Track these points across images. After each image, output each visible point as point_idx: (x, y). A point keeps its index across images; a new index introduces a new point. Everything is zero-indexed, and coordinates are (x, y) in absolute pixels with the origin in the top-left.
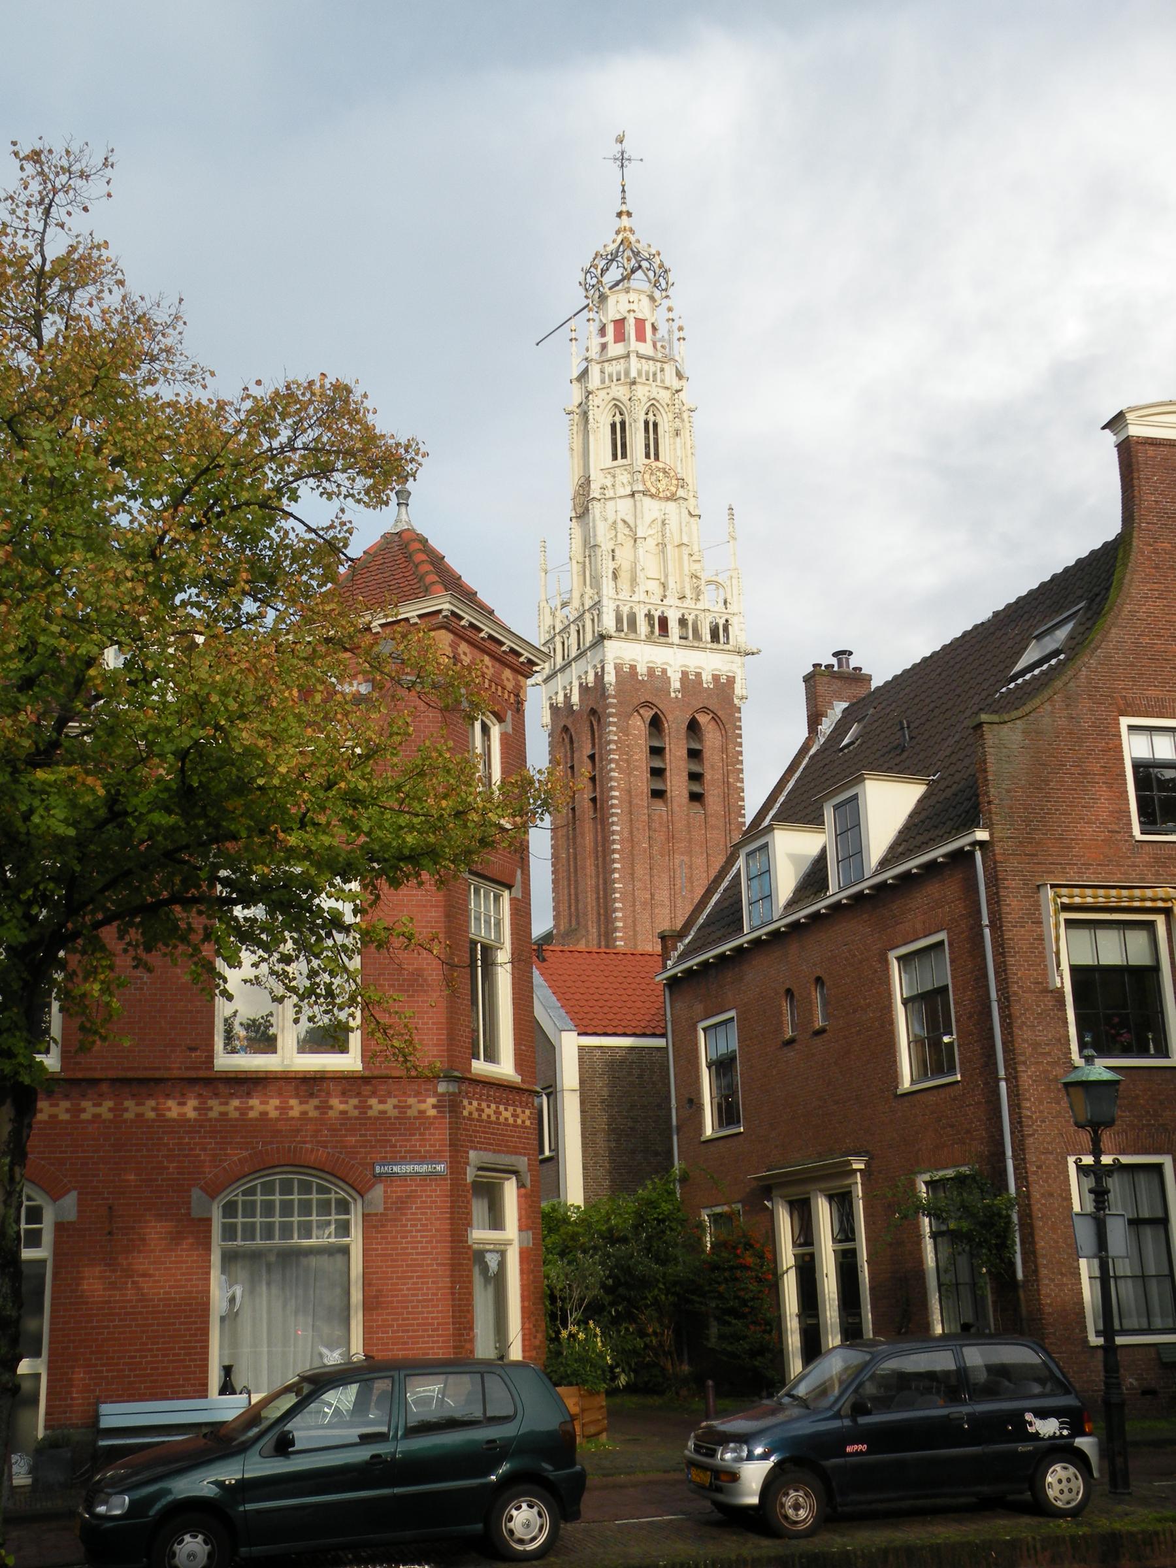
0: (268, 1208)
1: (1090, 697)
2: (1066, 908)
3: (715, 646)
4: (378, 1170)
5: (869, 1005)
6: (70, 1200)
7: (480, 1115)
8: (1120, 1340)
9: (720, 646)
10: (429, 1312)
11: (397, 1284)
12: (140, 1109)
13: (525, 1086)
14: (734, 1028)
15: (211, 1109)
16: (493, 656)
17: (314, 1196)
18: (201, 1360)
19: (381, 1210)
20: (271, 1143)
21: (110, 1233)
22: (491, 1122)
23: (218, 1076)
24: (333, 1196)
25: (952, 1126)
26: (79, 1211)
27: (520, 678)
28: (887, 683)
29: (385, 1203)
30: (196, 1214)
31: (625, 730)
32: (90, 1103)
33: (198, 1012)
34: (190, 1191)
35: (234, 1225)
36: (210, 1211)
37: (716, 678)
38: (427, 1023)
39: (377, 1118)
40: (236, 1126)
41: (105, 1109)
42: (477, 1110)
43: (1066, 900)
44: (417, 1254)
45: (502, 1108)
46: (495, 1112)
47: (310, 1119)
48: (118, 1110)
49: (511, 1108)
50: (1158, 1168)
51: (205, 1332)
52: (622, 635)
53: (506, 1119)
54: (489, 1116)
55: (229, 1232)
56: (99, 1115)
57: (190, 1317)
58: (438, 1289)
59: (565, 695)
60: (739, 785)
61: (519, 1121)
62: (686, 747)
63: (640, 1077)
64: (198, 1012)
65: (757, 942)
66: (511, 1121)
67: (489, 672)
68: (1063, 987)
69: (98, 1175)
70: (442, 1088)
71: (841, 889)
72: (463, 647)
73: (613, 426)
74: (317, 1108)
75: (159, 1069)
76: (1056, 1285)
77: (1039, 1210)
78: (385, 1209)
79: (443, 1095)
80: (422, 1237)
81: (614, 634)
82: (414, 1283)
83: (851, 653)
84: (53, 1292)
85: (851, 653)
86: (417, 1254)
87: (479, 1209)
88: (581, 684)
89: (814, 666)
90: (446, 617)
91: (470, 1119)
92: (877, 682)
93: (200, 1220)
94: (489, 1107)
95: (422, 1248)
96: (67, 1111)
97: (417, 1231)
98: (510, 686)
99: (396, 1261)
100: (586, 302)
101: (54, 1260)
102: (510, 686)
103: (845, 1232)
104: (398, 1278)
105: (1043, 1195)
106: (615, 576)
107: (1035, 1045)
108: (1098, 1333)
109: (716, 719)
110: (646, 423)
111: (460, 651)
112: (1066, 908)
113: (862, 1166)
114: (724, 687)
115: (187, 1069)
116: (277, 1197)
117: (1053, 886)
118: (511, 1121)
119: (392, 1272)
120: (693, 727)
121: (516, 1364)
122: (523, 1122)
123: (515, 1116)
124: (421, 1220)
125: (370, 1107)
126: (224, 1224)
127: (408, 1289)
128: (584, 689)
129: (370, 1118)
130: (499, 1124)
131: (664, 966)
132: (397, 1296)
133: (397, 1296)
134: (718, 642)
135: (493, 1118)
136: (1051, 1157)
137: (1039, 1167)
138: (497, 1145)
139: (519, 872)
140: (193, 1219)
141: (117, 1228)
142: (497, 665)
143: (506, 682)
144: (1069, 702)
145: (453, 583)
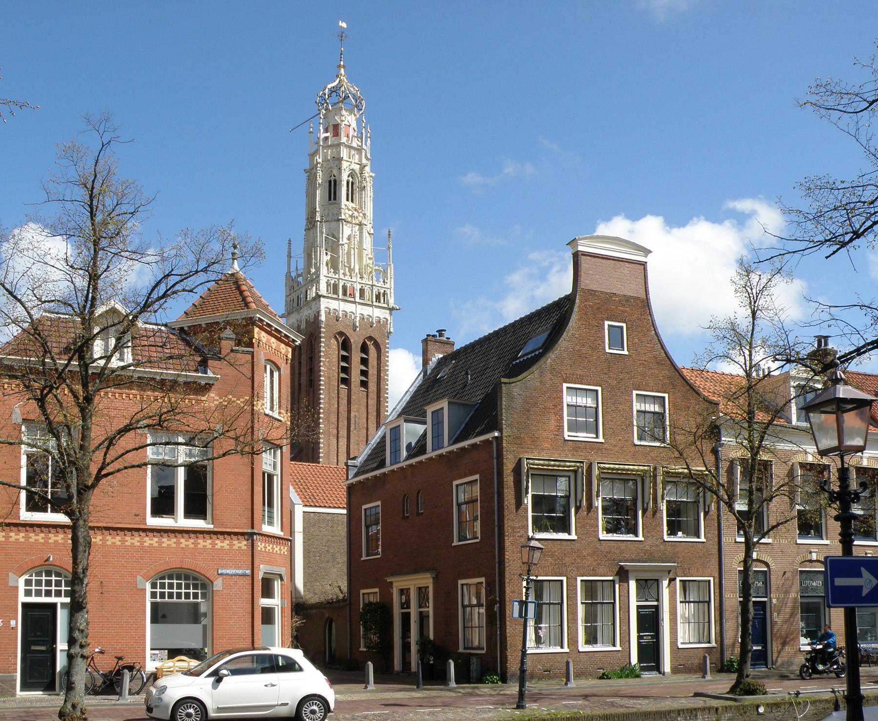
0: (171, 586)
3: (377, 304)
4: (220, 572)
12: (114, 540)
13: (285, 537)
15: (145, 542)
20: (172, 558)
21: (101, 593)
22: (270, 553)
30: (139, 586)
33: (139, 499)
39: (219, 549)
42: (264, 547)
46: (272, 548)
47: (190, 548)
49: (279, 547)
53: (277, 551)
54: (269, 550)
55: (154, 595)
58: (246, 623)
60: (386, 377)
64: (139, 499)
66: (279, 552)
73: (330, 182)
85: (445, 331)
88: (306, 320)
89: (428, 335)
92: (457, 347)
93: (141, 589)
94: (269, 546)
97: (237, 598)
107: (513, 528)
110: (348, 183)
111: (261, 336)
117: (527, 459)
120: (364, 349)
121: (30, 648)
122: (284, 553)
123: (280, 550)
124: (238, 594)
130: (274, 553)
131: (347, 479)
135: (271, 551)
138: (273, 563)
143: (282, 350)
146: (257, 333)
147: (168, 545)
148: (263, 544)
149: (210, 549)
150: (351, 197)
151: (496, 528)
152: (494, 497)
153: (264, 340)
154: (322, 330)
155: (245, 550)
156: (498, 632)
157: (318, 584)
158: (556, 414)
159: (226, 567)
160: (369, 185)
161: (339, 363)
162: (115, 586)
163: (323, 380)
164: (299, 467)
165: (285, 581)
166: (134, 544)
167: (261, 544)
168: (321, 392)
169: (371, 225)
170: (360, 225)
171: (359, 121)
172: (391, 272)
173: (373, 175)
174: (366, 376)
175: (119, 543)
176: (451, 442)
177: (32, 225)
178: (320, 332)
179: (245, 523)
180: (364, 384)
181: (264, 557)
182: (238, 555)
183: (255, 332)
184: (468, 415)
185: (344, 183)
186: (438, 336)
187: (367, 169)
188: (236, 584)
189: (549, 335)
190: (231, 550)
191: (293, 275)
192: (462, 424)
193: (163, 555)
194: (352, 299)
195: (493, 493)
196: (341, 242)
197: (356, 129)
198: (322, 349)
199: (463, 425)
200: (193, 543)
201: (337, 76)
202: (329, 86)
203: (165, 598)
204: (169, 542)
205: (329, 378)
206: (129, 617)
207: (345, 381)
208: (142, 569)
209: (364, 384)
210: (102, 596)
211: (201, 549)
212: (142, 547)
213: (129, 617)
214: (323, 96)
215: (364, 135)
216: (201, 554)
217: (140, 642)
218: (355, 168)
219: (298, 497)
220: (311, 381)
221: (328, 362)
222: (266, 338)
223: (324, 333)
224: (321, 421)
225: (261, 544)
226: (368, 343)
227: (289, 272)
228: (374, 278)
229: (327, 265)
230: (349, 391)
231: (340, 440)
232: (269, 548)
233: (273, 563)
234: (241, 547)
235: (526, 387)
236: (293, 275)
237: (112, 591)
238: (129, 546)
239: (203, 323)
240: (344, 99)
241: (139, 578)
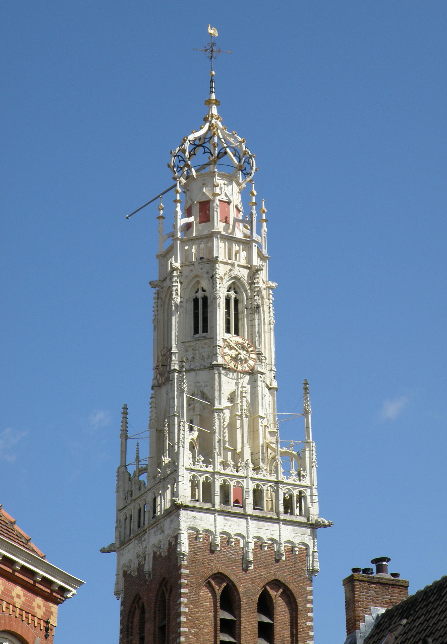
3: (287, 517)
28: (419, 593)
73: (196, 301)
85: (388, 560)
89: (355, 570)
92: (412, 591)
102: (40, 613)
106: (270, 324)
110: (228, 300)
134: (292, 513)
161: (216, 637)
169: (272, 374)
170: (252, 373)
173: (274, 285)
178: (179, 576)
185: (222, 302)
186: (375, 570)
187: (263, 275)
191: (132, 470)
194: (240, 510)
196: (217, 406)
198: (184, 609)
201: (206, 120)
214: (180, 153)
218: (240, 275)
221: (196, 634)
226: (273, 593)
236: (132, 470)
240: (218, 157)
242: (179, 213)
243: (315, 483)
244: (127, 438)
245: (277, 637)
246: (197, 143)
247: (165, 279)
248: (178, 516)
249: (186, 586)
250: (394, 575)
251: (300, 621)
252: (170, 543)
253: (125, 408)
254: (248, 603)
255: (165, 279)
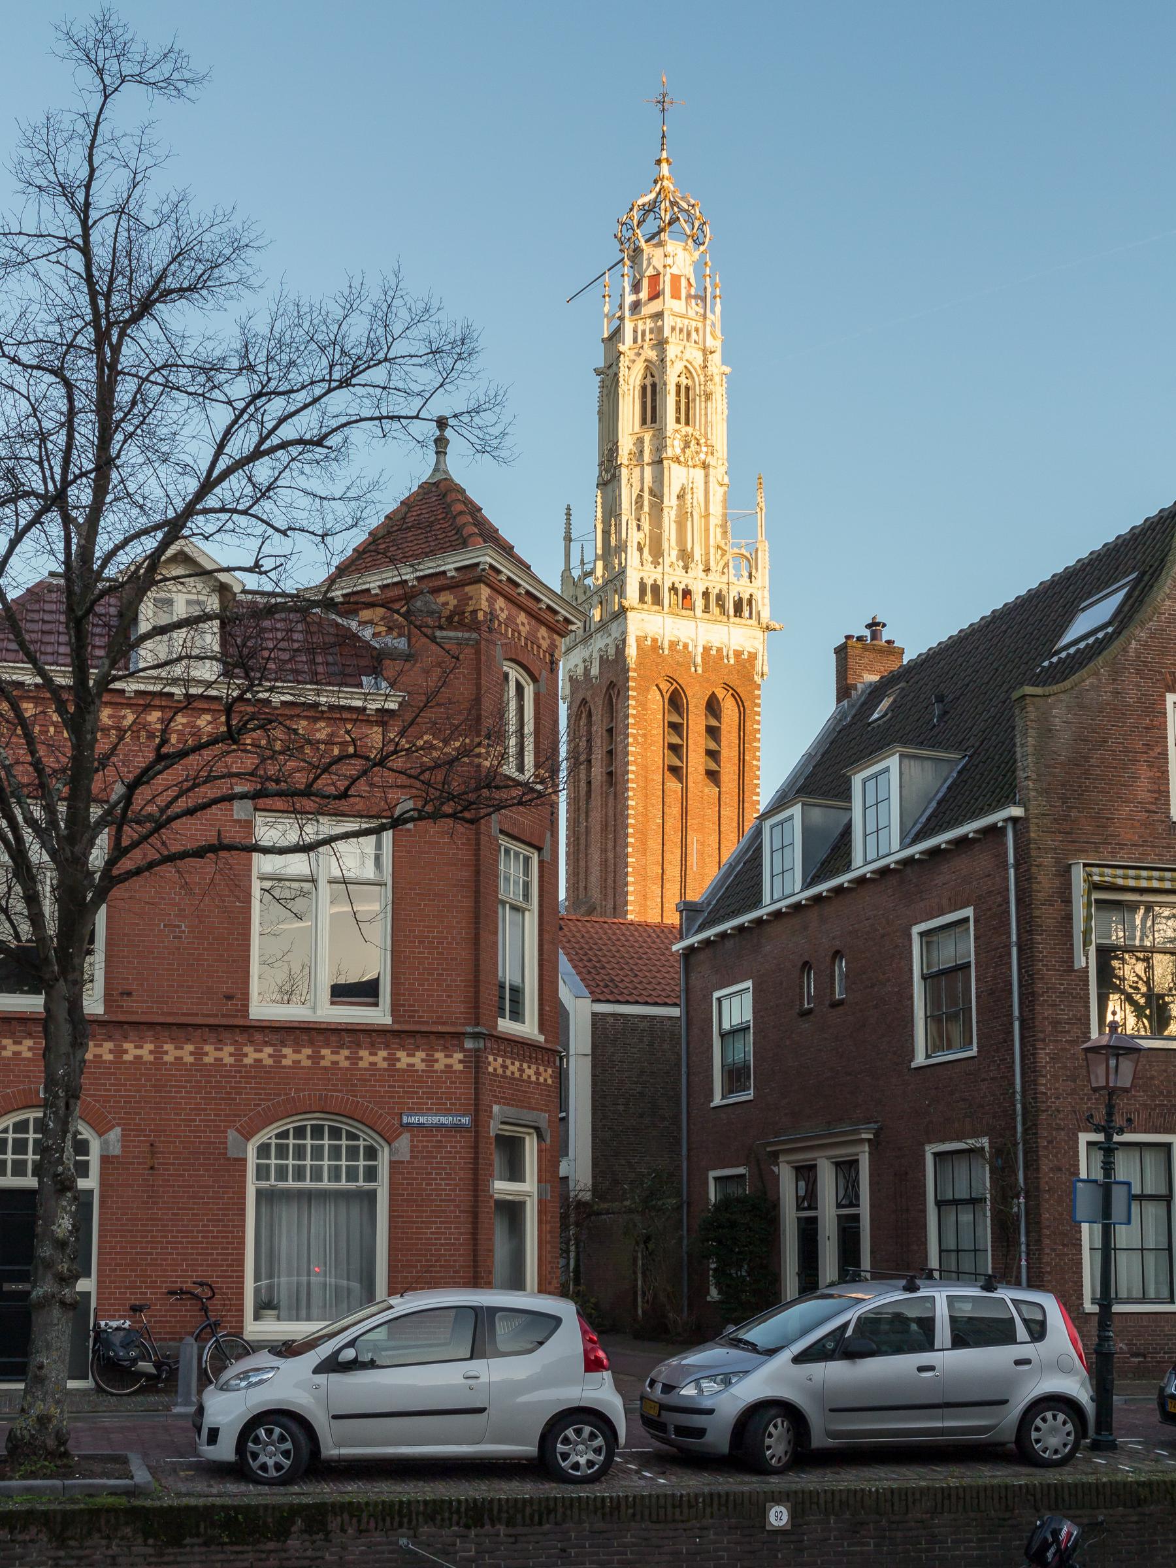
1: (1138, 672)
2: (1097, 887)
4: (405, 1120)
5: (889, 980)
6: (115, 1134)
7: (504, 1072)
8: (1117, 1308)
9: (743, 621)
10: (451, 1255)
11: (421, 1228)
12: (179, 1053)
13: (548, 1046)
14: (748, 998)
15: (246, 1055)
16: (530, 613)
17: (344, 1142)
18: (237, 1288)
19: (408, 1159)
20: (304, 1090)
21: (152, 1168)
22: (515, 1079)
23: (253, 1024)
24: (361, 1143)
25: (964, 1100)
26: (122, 1146)
27: (555, 636)
29: (412, 1151)
30: (232, 1153)
31: (643, 705)
32: (132, 1045)
34: (226, 1132)
35: (268, 1166)
36: (245, 1151)
37: (738, 654)
38: (455, 981)
39: (404, 1070)
40: (269, 1072)
41: (146, 1051)
43: (1096, 878)
44: (441, 1201)
45: (525, 1065)
48: (158, 1053)
49: (534, 1067)
50: (1168, 1146)
51: (707, 1183)
52: (645, 606)
53: (529, 1077)
54: (513, 1073)
55: (262, 1173)
56: (141, 1057)
57: (227, 1249)
58: (460, 1234)
59: (586, 668)
60: (755, 763)
61: (541, 1080)
62: (704, 723)
63: (651, 1044)
65: (778, 914)
66: (534, 1078)
67: (524, 630)
68: (1087, 967)
69: (140, 1114)
70: (469, 1044)
71: (866, 863)
72: (500, 603)
73: (644, 388)
74: (347, 1058)
75: (197, 1015)
76: (1057, 1255)
77: (1047, 1183)
78: (411, 1157)
79: (469, 1050)
80: (447, 1185)
81: (636, 606)
82: (438, 1228)
83: (884, 625)
84: (100, 1219)
85: (884, 625)
86: (441, 1201)
87: (497, 1161)
88: (601, 657)
89: (848, 637)
90: (484, 570)
91: (495, 1074)
93: (236, 1159)
94: (513, 1064)
95: (446, 1195)
96: (111, 1051)
97: (441, 1179)
98: (545, 644)
99: (422, 1206)
100: (620, 256)
101: (101, 1191)
102: (545, 644)
103: (849, 1197)
104: (422, 1222)
105: (1051, 1169)
107: (1056, 1023)
108: (1094, 1301)
109: (737, 697)
110: (678, 386)
112: (1097, 887)
113: (871, 1136)
114: (746, 664)
115: (223, 1016)
116: (309, 1142)
117: (1085, 865)
118: (534, 1078)
119: (417, 1217)
120: (713, 707)
122: (545, 1080)
123: (537, 1073)
124: (444, 1169)
125: (399, 1060)
126: (258, 1165)
127: (432, 1233)
128: (603, 661)
129: (399, 1070)
130: (523, 1081)
132: (421, 1239)
133: (421, 1239)
136: (1063, 1133)
137: (1050, 1142)
138: (520, 1101)
139: (548, 834)
140: (229, 1159)
141: (159, 1164)
142: (533, 622)
143: (541, 641)
144: (1116, 673)
145: (491, 536)
146: (487, 600)
147: (294, 1062)
148: (500, 1060)
149: (385, 1070)
150: (685, 416)
151: (1017, 1024)
152: (1010, 954)
153: (503, 616)
154: (631, 674)
155: (461, 1072)
156: (1024, 1263)
157: (623, 1162)
158: (1151, 765)
159: (420, 1112)
160: (719, 390)
162: (180, 1153)
163: (633, 772)
164: (584, 926)
165: (548, 1141)
166: (221, 1059)
167: (495, 1060)
168: (630, 794)
169: (724, 469)
170: (705, 466)
171: (699, 266)
172: (764, 558)
173: (728, 370)
174: (717, 739)
175: (190, 1059)
176: (908, 840)
177: (303, 787)
178: (627, 679)
179: (461, 1013)
180: (713, 776)
181: (501, 1087)
182: (445, 1082)
183: (484, 597)
184: (945, 781)
185: (671, 388)
187: (716, 359)
188: (439, 1146)
189: (1128, 596)
190: (430, 1071)
191: (576, 573)
192: (929, 803)
193: (285, 1084)
195: (1008, 946)
197: (693, 281)
198: (632, 711)
199: (934, 804)
200: (347, 1058)
202: (640, 202)
203: (268, 1179)
204: (297, 1057)
205: (645, 767)
206: (209, 1220)
207: (675, 771)
208: (239, 1116)
209: (713, 776)
210: (152, 1175)
211: (366, 1069)
212: (239, 1066)
213: (209, 1220)
214: (628, 221)
215: (709, 290)
216: (365, 1080)
217: (231, 1277)
219: (582, 984)
220: (610, 774)
221: (644, 735)
222: (506, 612)
223: (635, 679)
224: (630, 869)
225: (495, 1060)
227: (568, 569)
228: (732, 571)
229: (640, 549)
230: (685, 791)
231: (666, 886)
232: (513, 1068)
233: (520, 1101)
234: (451, 1066)
235: (1081, 707)
236: (576, 573)
237: (174, 1164)
238: (211, 1065)
239: (371, 585)
240: (670, 224)
241: (232, 1135)
242: (628, 289)
243: (767, 585)
244: (570, 540)
245: (723, 739)
246: (646, 208)
247: (611, 366)
248: (626, 619)
249: (634, 689)
250: (888, 642)
251: (748, 724)
252: (617, 647)
253: (569, 509)
254: (696, 706)
255: (611, 366)
